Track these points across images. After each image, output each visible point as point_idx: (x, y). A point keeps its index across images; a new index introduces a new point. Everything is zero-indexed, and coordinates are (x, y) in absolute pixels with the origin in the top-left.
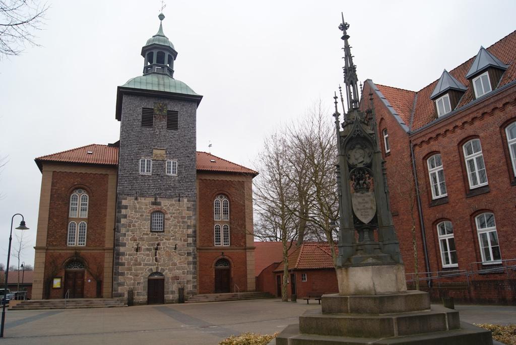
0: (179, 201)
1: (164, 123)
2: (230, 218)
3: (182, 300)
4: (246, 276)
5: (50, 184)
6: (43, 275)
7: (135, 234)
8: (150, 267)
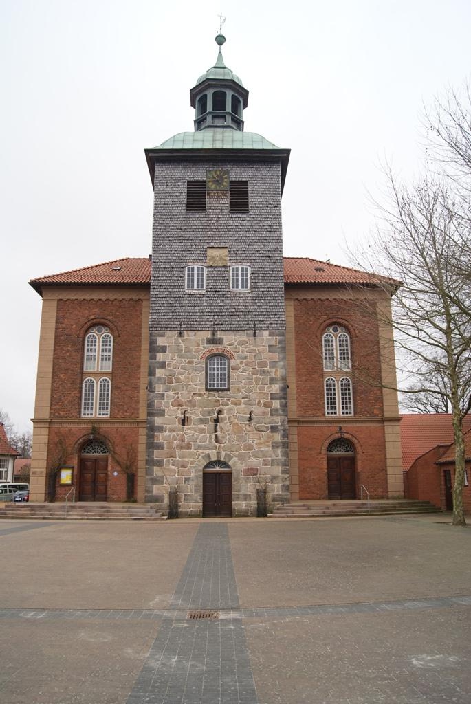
0: (255, 334)
1: (225, 202)
2: (352, 366)
3: (262, 511)
4: (384, 470)
5: (54, 320)
6: (45, 464)
7: (180, 395)
8: (206, 452)
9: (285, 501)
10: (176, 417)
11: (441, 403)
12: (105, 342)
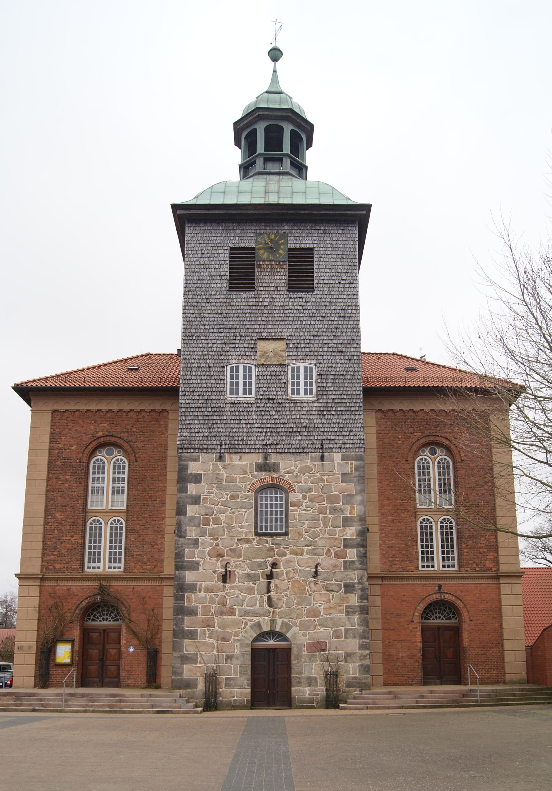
0: (322, 458)
2: (456, 501)
4: (500, 644)
8: (256, 619)
9: (364, 686)
10: (214, 572)
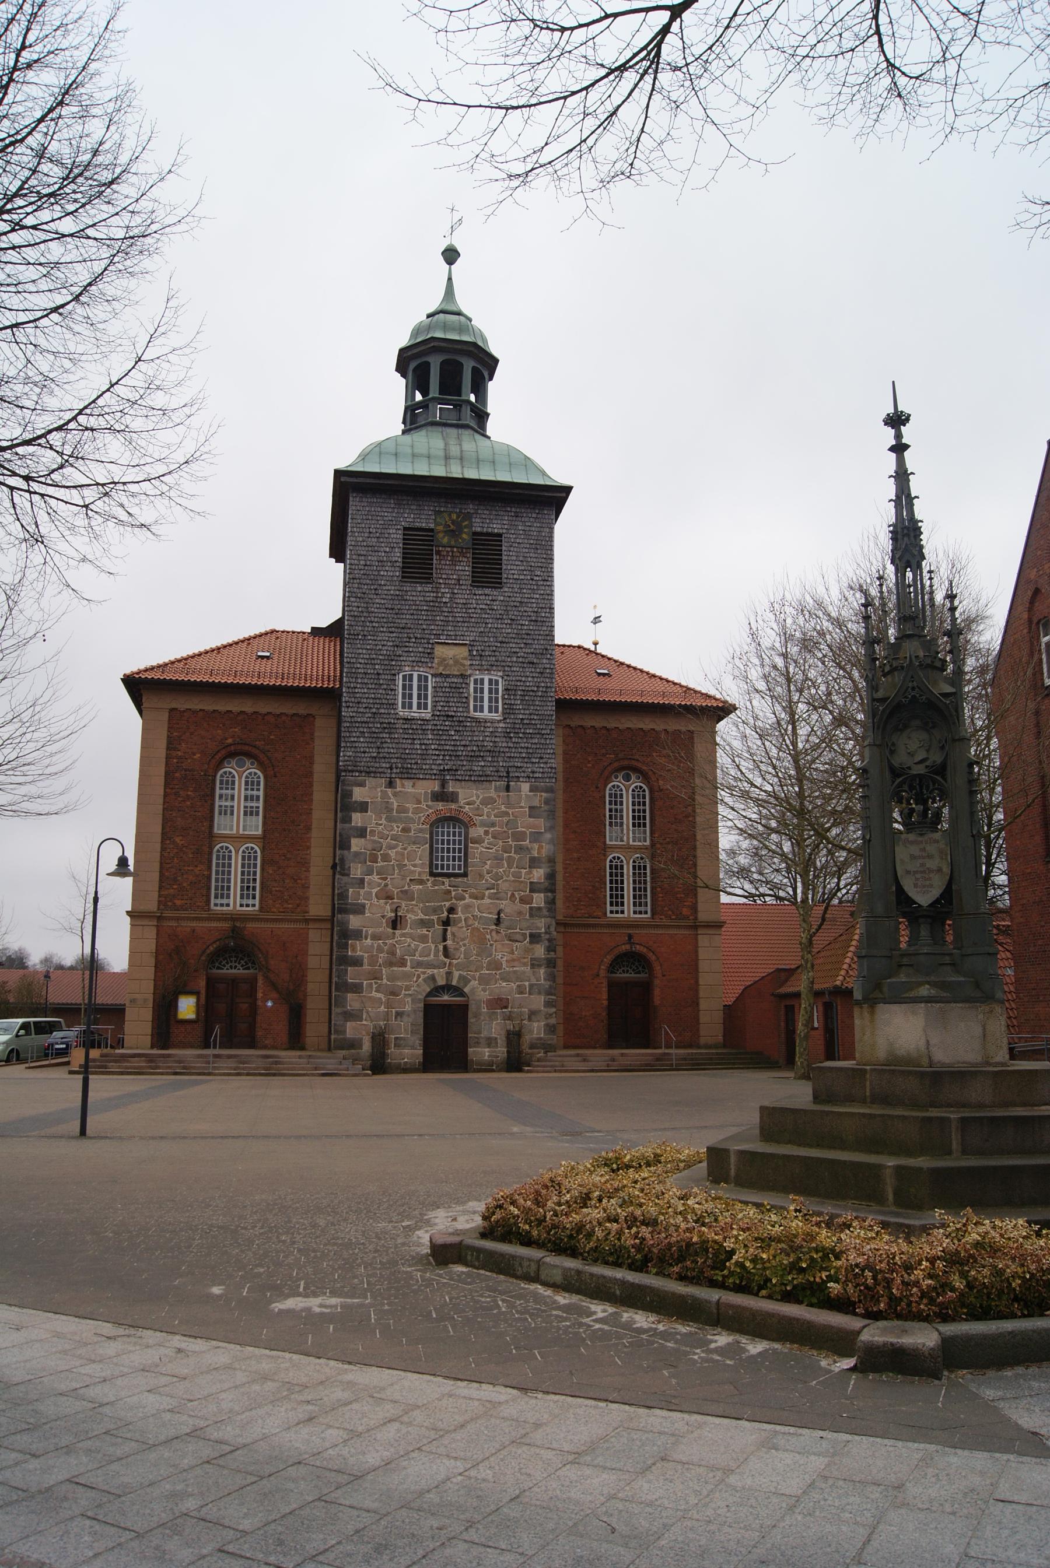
0: (508, 789)
1: (465, 568)
3: (515, 1063)
6: (152, 987)
8: (430, 971)
9: (548, 1048)
10: (383, 917)
11: (785, 881)
12: (250, 784)
